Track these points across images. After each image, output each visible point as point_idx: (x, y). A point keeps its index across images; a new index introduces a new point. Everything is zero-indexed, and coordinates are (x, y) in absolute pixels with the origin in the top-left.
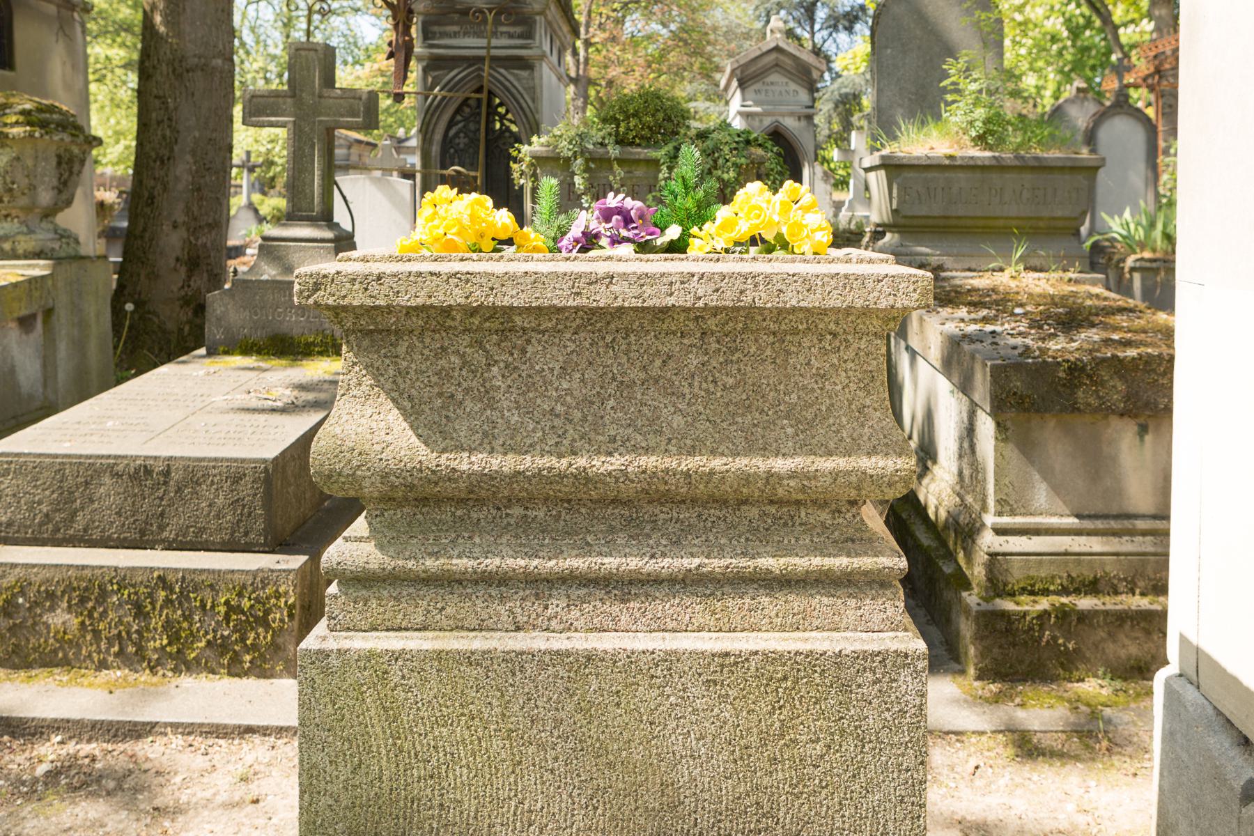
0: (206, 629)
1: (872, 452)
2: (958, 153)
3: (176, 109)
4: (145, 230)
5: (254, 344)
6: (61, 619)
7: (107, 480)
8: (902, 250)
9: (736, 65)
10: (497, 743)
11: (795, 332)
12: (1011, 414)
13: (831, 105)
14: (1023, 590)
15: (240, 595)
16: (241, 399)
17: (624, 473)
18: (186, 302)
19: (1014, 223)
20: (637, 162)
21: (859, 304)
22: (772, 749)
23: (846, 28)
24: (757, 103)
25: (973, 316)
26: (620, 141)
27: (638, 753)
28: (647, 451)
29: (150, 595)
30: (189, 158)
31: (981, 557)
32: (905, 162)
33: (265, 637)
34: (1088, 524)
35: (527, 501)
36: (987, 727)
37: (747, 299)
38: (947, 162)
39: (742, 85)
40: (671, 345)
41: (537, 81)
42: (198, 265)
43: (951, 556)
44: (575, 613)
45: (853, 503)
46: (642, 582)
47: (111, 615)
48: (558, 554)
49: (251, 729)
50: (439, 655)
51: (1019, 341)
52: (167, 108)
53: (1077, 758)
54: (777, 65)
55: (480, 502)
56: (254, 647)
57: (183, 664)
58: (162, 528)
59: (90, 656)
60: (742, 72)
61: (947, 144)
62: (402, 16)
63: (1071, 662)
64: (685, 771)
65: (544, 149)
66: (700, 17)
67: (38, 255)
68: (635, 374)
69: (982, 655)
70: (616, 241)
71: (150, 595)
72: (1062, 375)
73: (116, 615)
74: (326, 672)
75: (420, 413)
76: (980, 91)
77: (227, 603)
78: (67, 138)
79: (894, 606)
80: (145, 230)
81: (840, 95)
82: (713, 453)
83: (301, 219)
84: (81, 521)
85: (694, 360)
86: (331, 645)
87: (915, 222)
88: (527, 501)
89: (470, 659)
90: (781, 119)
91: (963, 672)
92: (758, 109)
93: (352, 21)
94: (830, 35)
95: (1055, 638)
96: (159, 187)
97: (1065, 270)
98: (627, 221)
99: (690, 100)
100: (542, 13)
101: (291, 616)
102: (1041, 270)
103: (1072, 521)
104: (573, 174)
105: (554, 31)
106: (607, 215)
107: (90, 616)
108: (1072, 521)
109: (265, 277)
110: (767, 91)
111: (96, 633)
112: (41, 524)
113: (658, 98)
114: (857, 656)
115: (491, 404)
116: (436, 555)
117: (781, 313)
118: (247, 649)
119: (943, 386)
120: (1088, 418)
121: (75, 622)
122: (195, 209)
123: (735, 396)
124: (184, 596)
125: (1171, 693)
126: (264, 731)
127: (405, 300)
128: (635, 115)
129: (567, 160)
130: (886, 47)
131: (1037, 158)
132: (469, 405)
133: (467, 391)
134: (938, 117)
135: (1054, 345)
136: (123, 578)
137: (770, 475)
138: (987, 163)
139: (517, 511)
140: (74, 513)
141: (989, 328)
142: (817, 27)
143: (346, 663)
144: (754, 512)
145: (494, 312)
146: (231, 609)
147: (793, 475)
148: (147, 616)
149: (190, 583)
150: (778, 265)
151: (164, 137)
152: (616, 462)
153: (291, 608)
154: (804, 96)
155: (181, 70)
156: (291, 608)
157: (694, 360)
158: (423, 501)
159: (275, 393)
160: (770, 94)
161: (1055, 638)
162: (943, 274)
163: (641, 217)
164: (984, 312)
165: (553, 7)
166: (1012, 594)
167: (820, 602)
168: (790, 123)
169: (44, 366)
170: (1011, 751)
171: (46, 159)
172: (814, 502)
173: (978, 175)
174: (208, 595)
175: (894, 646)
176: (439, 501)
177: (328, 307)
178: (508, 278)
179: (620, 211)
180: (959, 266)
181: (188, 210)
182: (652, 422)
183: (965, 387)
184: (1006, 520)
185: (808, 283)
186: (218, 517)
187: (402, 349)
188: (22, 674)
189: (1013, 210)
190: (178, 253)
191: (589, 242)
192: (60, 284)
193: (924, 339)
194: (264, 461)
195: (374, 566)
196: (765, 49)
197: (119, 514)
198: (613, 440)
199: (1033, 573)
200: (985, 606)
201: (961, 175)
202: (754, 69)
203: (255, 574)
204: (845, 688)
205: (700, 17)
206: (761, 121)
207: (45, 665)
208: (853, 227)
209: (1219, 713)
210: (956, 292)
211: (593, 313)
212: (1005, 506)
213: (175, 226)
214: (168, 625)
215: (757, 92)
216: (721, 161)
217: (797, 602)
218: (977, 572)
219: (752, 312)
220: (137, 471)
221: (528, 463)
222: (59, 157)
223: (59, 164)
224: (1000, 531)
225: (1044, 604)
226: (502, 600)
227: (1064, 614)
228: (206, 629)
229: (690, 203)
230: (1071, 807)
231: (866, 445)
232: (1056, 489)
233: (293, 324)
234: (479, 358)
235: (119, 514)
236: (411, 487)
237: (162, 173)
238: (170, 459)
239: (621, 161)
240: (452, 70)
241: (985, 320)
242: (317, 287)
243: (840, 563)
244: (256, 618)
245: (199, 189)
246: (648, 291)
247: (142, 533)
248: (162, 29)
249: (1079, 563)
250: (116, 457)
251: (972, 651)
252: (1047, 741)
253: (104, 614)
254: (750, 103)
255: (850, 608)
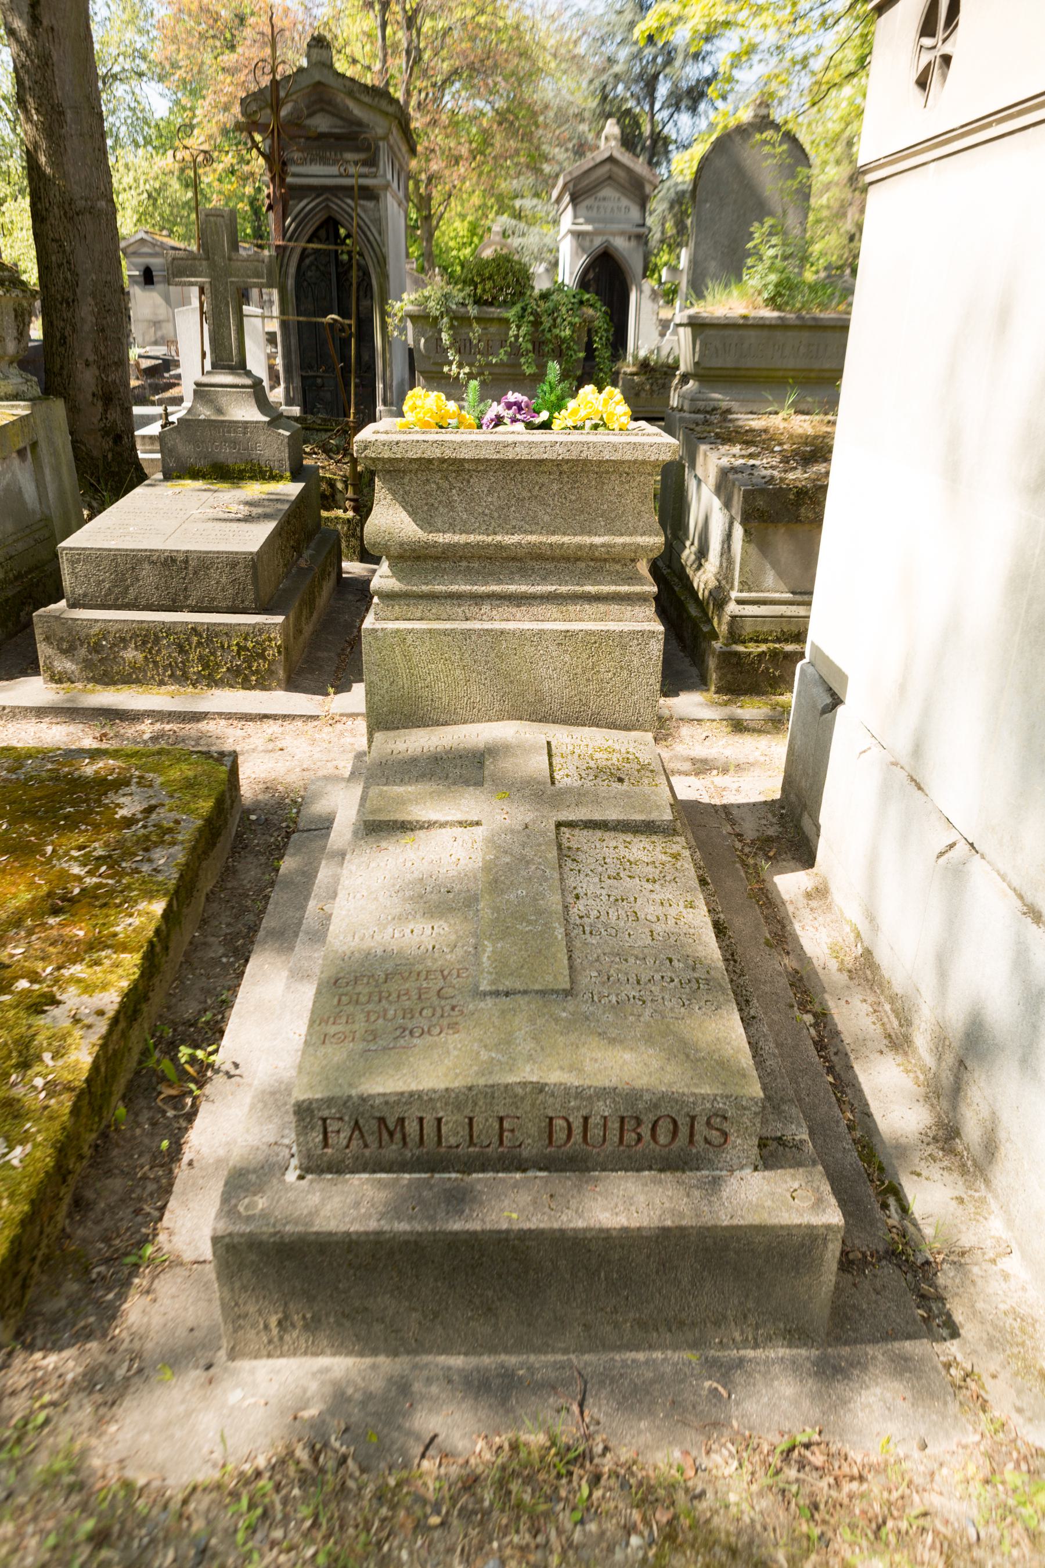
0: (226, 661)
1: (643, 534)
2: (753, 313)
3: (72, 252)
4: (62, 368)
5: (199, 471)
6: (130, 654)
7: (146, 566)
8: (701, 396)
9: (568, 178)
10: (458, 672)
11: (607, 472)
12: (754, 524)
13: (665, 205)
14: (751, 640)
15: (245, 639)
16: (211, 513)
17: (520, 544)
18: (106, 432)
19: (791, 373)
20: (492, 320)
21: (640, 458)
22: (589, 675)
23: (688, 108)
24: (588, 221)
25: (744, 452)
26: (478, 301)
27: (525, 677)
28: (531, 533)
29: (187, 639)
30: (90, 299)
31: (726, 619)
32: (707, 321)
33: (264, 666)
34: (798, 598)
35: (469, 558)
36: (717, 717)
37: (584, 455)
38: (741, 322)
39: (575, 200)
40: (544, 479)
41: (382, 212)
42: (111, 400)
43: (709, 621)
44: (494, 612)
45: (633, 560)
46: (527, 598)
47: (164, 652)
48: (486, 584)
49: (266, 717)
50: (430, 631)
51: (769, 472)
52: (64, 251)
53: (768, 733)
54: (610, 178)
55: (446, 559)
56: (257, 672)
57: (214, 682)
58: (186, 598)
59: (153, 677)
60: (575, 186)
61: (744, 304)
62: (277, 168)
63: (776, 683)
64: (546, 684)
65: (416, 308)
66: (527, 91)
67: (16, 397)
68: (526, 494)
69: (720, 679)
70: (514, 420)
71: (187, 639)
72: (792, 497)
73: (166, 652)
74: (376, 639)
75: (416, 514)
76: (776, 257)
77: (238, 644)
78: (21, 295)
79: (650, 610)
80: (62, 368)
81: (677, 193)
82: (564, 534)
83: (223, 367)
84: (132, 593)
85: (555, 487)
86: (379, 625)
87: (712, 373)
88: (469, 558)
89: (445, 633)
90: (611, 239)
91: (708, 690)
92: (588, 228)
93: (137, 90)
94: (672, 116)
95: (767, 669)
96: (68, 328)
97: (826, 414)
98: (520, 409)
99: (516, 197)
100: (385, 138)
101: (279, 652)
102: (808, 413)
103: (788, 596)
104: (440, 331)
105: (394, 153)
106: (509, 406)
107: (150, 653)
108: (788, 596)
109: (202, 417)
110: (598, 208)
111: (155, 663)
112: (106, 595)
113: (509, 261)
114: (630, 633)
115: (453, 509)
116: (427, 584)
117: (600, 463)
118: (253, 673)
119: (717, 503)
120: (807, 527)
121: (140, 656)
122: (102, 348)
123: (576, 506)
124: (209, 640)
125: (802, 670)
126: (274, 717)
127: (410, 455)
128: (490, 278)
129: (436, 318)
130: (706, 201)
131: (815, 319)
132: (441, 509)
133: (440, 502)
134: (739, 279)
135: (791, 476)
136: (169, 629)
137: (592, 545)
138: (774, 322)
139: (464, 564)
140: (127, 588)
141: (752, 462)
142: (657, 106)
143: (386, 635)
144: (583, 565)
145: (454, 461)
146: (241, 648)
147: (603, 545)
148: (186, 652)
149: (213, 632)
150: (601, 437)
151: (66, 280)
152: (515, 538)
153: (279, 647)
154: (635, 213)
155: (71, 214)
156: (279, 647)
157: (555, 487)
158: (418, 558)
159: (234, 508)
160: (602, 210)
161: (767, 669)
162: (731, 417)
163: (527, 406)
164: (752, 450)
165: (394, 130)
166: (743, 642)
167: (614, 608)
168: (620, 244)
169: (37, 487)
170: (729, 729)
171: (8, 314)
172: (614, 559)
173: (765, 333)
174: (225, 639)
175: (648, 628)
176: (426, 558)
177: (371, 458)
178: (463, 443)
179: (515, 404)
180: (743, 410)
181: (96, 350)
182: (534, 518)
183: (727, 505)
184: (745, 595)
185: (615, 447)
186: (223, 590)
187: (406, 480)
188: (112, 688)
189: (791, 363)
190: (94, 389)
191: (498, 421)
192: (38, 421)
193: (706, 470)
194: (251, 553)
195: (396, 589)
196: (598, 160)
197: (157, 588)
198: (514, 527)
199: (758, 629)
200: (725, 649)
201: (752, 333)
202: (586, 182)
203: (254, 626)
204: (624, 647)
205: (527, 91)
206: (592, 241)
207: (125, 683)
208: (671, 361)
209: (821, 677)
210: (737, 432)
211: (505, 462)
212: (745, 586)
213: (87, 365)
214: (201, 658)
215: (589, 208)
216: (559, 320)
217: (602, 607)
218: (723, 629)
219: (586, 462)
220: (166, 560)
221: (472, 538)
222: (15, 310)
223: (16, 316)
224: (740, 602)
225: (763, 647)
226: (459, 606)
227: (774, 654)
228: (226, 661)
229: (553, 398)
230: (757, 754)
231: (640, 531)
232: (780, 575)
233: (226, 454)
234: (445, 485)
235: (157, 588)
236: (414, 550)
237: (69, 315)
238: (187, 552)
239: (479, 320)
240: (301, 200)
241: (751, 456)
242: (366, 448)
243: (624, 589)
244: (258, 654)
245: (103, 330)
246: (534, 450)
247: (174, 601)
248: (48, 170)
249: (790, 623)
250: (151, 551)
251: (714, 676)
252: (752, 725)
253: (159, 651)
254: (581, 220)
255: (628, 610)
